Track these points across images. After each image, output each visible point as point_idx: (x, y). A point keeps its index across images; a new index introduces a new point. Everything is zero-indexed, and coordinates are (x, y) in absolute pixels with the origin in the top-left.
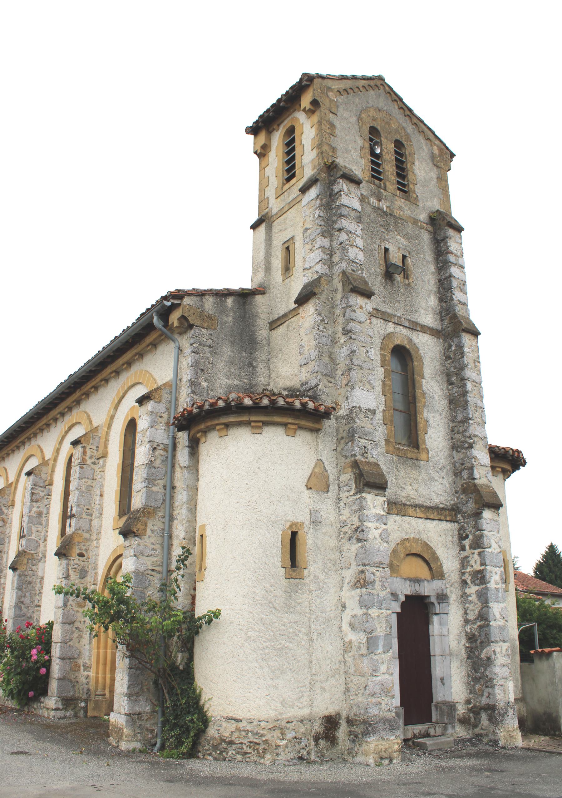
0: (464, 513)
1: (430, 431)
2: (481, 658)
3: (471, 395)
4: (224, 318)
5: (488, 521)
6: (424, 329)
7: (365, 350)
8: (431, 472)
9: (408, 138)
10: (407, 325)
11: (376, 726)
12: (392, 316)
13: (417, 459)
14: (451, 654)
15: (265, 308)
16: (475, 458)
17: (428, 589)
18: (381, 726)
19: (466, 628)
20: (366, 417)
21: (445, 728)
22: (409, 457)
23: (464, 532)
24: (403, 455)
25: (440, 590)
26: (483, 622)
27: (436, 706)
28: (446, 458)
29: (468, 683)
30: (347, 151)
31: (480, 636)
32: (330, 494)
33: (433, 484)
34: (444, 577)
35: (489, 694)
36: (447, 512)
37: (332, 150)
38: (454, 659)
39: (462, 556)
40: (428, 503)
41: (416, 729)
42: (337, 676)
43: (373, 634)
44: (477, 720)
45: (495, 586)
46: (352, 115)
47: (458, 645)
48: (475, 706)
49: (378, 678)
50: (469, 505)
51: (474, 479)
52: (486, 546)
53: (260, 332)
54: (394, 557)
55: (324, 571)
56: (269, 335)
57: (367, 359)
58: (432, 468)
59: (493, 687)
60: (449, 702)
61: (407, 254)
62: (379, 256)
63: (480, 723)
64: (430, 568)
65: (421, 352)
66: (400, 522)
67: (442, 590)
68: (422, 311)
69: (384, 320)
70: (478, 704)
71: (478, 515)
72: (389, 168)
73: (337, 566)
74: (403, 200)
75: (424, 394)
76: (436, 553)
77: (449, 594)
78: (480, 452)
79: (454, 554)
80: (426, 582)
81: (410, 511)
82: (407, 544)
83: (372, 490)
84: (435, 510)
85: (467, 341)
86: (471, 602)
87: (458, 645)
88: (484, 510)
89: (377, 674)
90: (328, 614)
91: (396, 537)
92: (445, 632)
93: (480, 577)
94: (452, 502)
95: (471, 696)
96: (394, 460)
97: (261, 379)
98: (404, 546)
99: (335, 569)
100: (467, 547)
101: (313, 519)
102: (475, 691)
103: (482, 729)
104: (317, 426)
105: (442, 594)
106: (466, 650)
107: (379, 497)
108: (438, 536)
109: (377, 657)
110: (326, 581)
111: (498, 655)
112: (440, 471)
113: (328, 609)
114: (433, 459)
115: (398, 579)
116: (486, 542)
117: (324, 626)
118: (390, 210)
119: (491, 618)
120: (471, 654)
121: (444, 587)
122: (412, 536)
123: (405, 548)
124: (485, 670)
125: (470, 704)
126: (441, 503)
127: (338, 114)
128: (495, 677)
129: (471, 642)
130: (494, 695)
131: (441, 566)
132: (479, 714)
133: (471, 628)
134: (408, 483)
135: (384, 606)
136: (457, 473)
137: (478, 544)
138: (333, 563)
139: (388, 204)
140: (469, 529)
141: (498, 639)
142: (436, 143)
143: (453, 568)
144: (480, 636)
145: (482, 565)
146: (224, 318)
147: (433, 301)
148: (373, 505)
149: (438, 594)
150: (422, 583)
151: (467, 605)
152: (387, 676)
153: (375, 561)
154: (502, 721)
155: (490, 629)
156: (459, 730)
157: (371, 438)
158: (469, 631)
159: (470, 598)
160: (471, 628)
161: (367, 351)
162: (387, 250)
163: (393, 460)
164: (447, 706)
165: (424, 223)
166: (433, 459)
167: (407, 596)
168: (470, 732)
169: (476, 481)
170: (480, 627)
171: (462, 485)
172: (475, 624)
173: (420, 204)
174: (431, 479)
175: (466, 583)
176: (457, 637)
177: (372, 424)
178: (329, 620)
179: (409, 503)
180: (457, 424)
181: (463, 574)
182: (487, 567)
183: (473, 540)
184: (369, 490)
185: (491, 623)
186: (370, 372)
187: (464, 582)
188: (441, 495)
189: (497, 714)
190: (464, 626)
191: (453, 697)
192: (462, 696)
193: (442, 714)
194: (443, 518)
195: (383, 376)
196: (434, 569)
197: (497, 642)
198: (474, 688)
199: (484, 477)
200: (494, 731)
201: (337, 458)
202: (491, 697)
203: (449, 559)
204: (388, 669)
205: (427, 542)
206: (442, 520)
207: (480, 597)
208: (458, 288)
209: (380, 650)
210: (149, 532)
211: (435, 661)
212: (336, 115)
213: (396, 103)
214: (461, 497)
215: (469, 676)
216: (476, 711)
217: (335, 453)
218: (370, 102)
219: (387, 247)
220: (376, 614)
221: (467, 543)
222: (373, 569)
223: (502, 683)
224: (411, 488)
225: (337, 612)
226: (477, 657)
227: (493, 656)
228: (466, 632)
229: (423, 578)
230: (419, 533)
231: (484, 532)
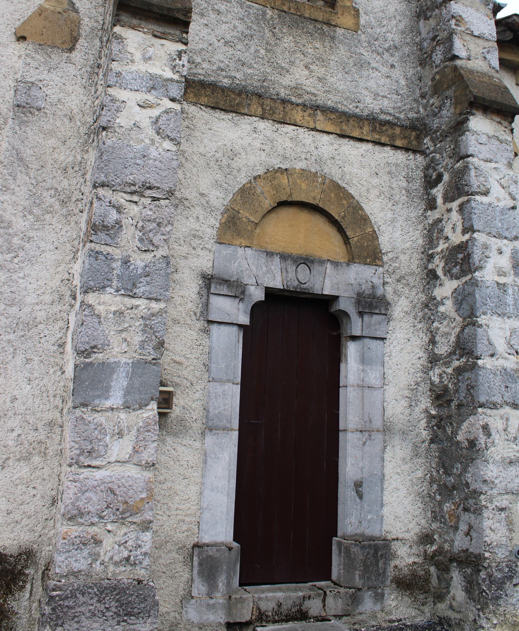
0: (436, 132)
2: (458, 443)
5: (484, 139)
8: (362, 51)
11: (70, 603)
13: (328, 24)
14: (387, 429)
16: (459, 20)
18: (87, 604)
19: (431, 373)
21: (355, 600)
22: (307, 15)
23: (435, 170)
24: (292, 11)
25: (366, 288)
26: (464, 360)
27: (339, 544)
28: (403, 32)
29: (430, 496)
31: (457, 391)
32: (77, 55)
33: (365, 73)
34: (381, 259)
35: (470, 527)
36: (398, 131)
38: (397, 441)
39: (431, 222)
40: (350, 108)
41: (267, 599)
42: (36, 459)
43: (94, 356)
44: (443, 585)
45: (497, 278)
47: (408, 411)
48: (440, 551)
49: (99, 474)
50: (444, 112)
51: (456, 57)
52: (475, 189)
54: (244, 203)
55: (30, 213)
58: (365, 44)
59: (478, 511)
60: (372, 539)
63: (449, 592)
64: (346, 240)
66: (268, 133)
67: (373, 287)
70: (446, 546)
71: (459, 127)
73: (72, 206)
76: (361, 208)
77: (390, 296)
79: (412, 215)
80: (329, 265)
81: (298, 115)
82: (284, 180)
83: (143, 24)
84: (366, 123)
86: (444, 317)
87: (408, 411)
88: (473, 114)
89: (94, 463)
90: (27, 310)
92: (373, 377)
93: (462, 261)
94: (411, 115)
95: (434, 526)
96: (268, 16)
98: (276, 182)
99: (64, 211)
100: (440, 201)
101: (22, 99)
102: (443, 517)
103: (451, 607)
105: (373, 296)
106: (428, 422)
107: (163, 42)
108: (374, 178)
109: (100, 418)
110: (31, 234)
111: (495, 436)
113: (31, 299)
115: (249, 251)
116: (474, 180)
117: (12, 337)
119: (481, 348)
120: (439, 432)
121: (376, 281)
122: (300, 165)
123: (277, 188)
124: (465, 470)
125: (432, 543)
126: (382, 112)
128: (485, 488)
129: (440, 406)
130: (481, 532)
131: (374, 236)
132: (447, 570)
133: (440, 375)
135: (140, 290)
136: (424, 60)
137: (459, 189)
138: (62, 198)
140: (444, 162)
141: (497, 399)
143: (408, 245)
144: (457, 391)
145: (465, 231)
148: (143, 55)
149: (359, 294)
150: (316, 268)
151: (436, 324)
152: (132, 471)
153: (130, 179)
154: (498, 598)
155: (477, 375)
156: (394, 604)
158: (436, 379)
159: (442, 309)
160: (440, 375)
163: (264, 14)
164: (363, 547)
167: (269, 292)
168: (426, 609)
169: (458, 63)
170: (459, 371)
172: (447, 364)
174: (361, 64)
175: (436, 277)
176: (406, 393)
178: (30, 325)
179: (300, 101)
181: (431, 257)
182: (475, 235)
183: (451, 181)
184: (135, 22)
185: (480, 362)
187: (432, 276)
188: (384, 97)
189: (484, 580)
190: (426, 371)
191: (385, 528)
192: (411, 526)
193: (349, 565)
194: (383, 140)
196: (353, 241)
197: (494, 406)
198: (442, 510)
200: (475, 620)
202: (474, 534)
203: (398, 225)
204: (136, 451)
205: (340, 182)
206: (384, 145)
207: (461, 304)
209: (116, 399)
211: (346, 441)
215: (432, 481)
216: (443, 561)
220: (113, 308)
221: (438, 192)
222: (121, 198)
223: (504, 503)
224: (306, 72)
225: (56, 308)
226: (451, 439)
227: (482, 439)
228: (432, 383)
229: (325, 257)
230: (319, 161)
231: (470, 159)
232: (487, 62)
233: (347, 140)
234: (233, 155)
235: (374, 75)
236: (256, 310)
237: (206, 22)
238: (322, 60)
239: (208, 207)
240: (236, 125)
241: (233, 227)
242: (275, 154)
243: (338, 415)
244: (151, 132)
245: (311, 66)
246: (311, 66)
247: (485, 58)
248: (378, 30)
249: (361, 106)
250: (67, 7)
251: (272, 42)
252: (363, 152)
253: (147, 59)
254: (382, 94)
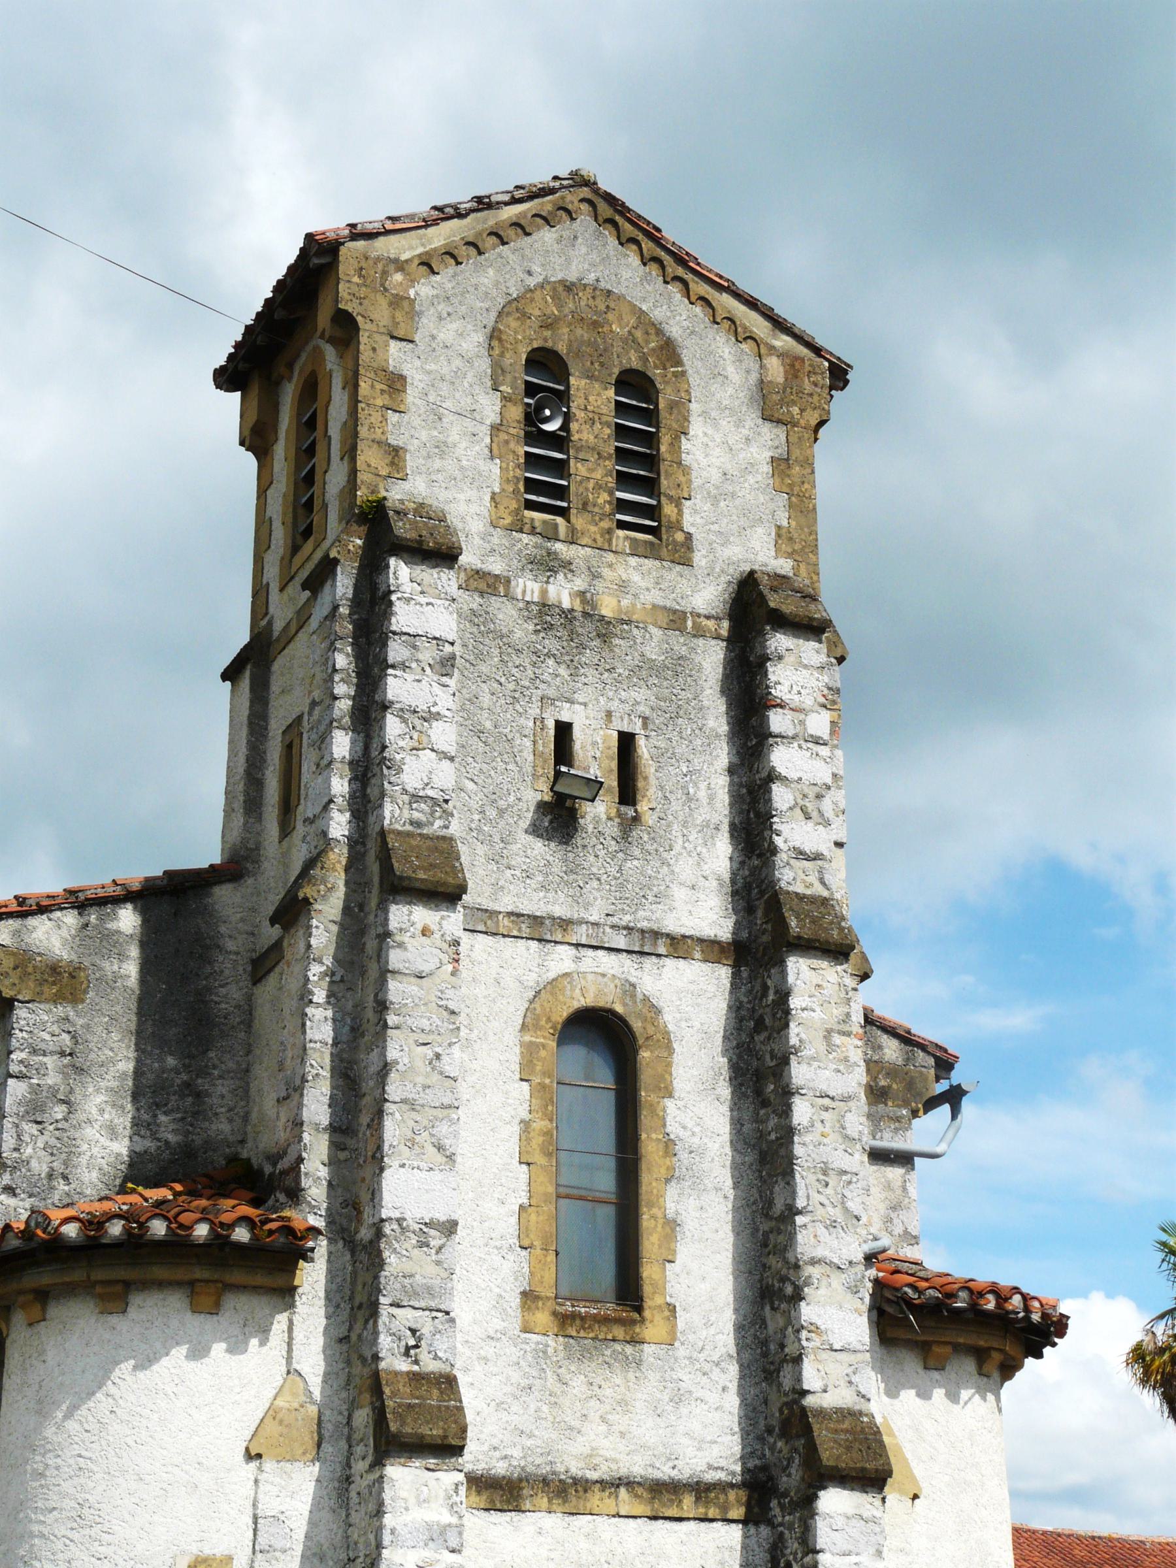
1: (685, 1252)
3: (808, 1138)
4: (110, 967)
6: (679, 946)
7: (430, 1054)
9: (669, 352)
10: (621, 942)
15: (242, 920)
20: (423, 1244)
30: (442, 448)
37: (388, 459)
40: (664, 1472)
46: (470, 327)
53: (223, 991)
56: (249, 998)
57: (435, 1077)
61: (636, 727)
62: (532, 748)
69: (540, 940)
74: (633, 561)
75: (669, 1146)
78: (832, 1310)
85: (806, 973)
96: (550, 1351)
97: (222, 1126)
104: (279, 1281)
112: (716, 1370)
114: (691, 1337)
118: (584, 601)
127: (417, 339)
134: (594, 1416)
139: (580, 584)
142: (777, 343)
146: (110, 967)
147: (720, 855)
157: (433, 1304)
161: (438, 1056)
165: (708, 617)
166: (691, 1337)
171: (781, 1411)
177: (438, 1263)
180: (773, 1223)
186: (439, 1113)
195: (526, 1106)
199: (843, 1383)
201: (348, 1362)
206: (712, 1520)
208: (798, 811)
212: (412, 342)
213: (634, 247)
214: (780, 1444)
217: (345, 1347)
218: (536, 268)
219: (565, 717)
232: (853, 1388)
233: (661, 1522)
235: (698, 1411)
237: (470, 1380)
238: (623, 1404)
240: (516, 1529)
242: (567, 1562)
243: (1094, 1542)
245: (609, 1416)
246: (609, 1416)
247: (850, 1382)
248: (704, 1333)
249: (680, 1464)
250: (304, 1399)
251: (558, 1388)
252: (684, 1537)
253: (422, 1502)
254: (709, 1438)
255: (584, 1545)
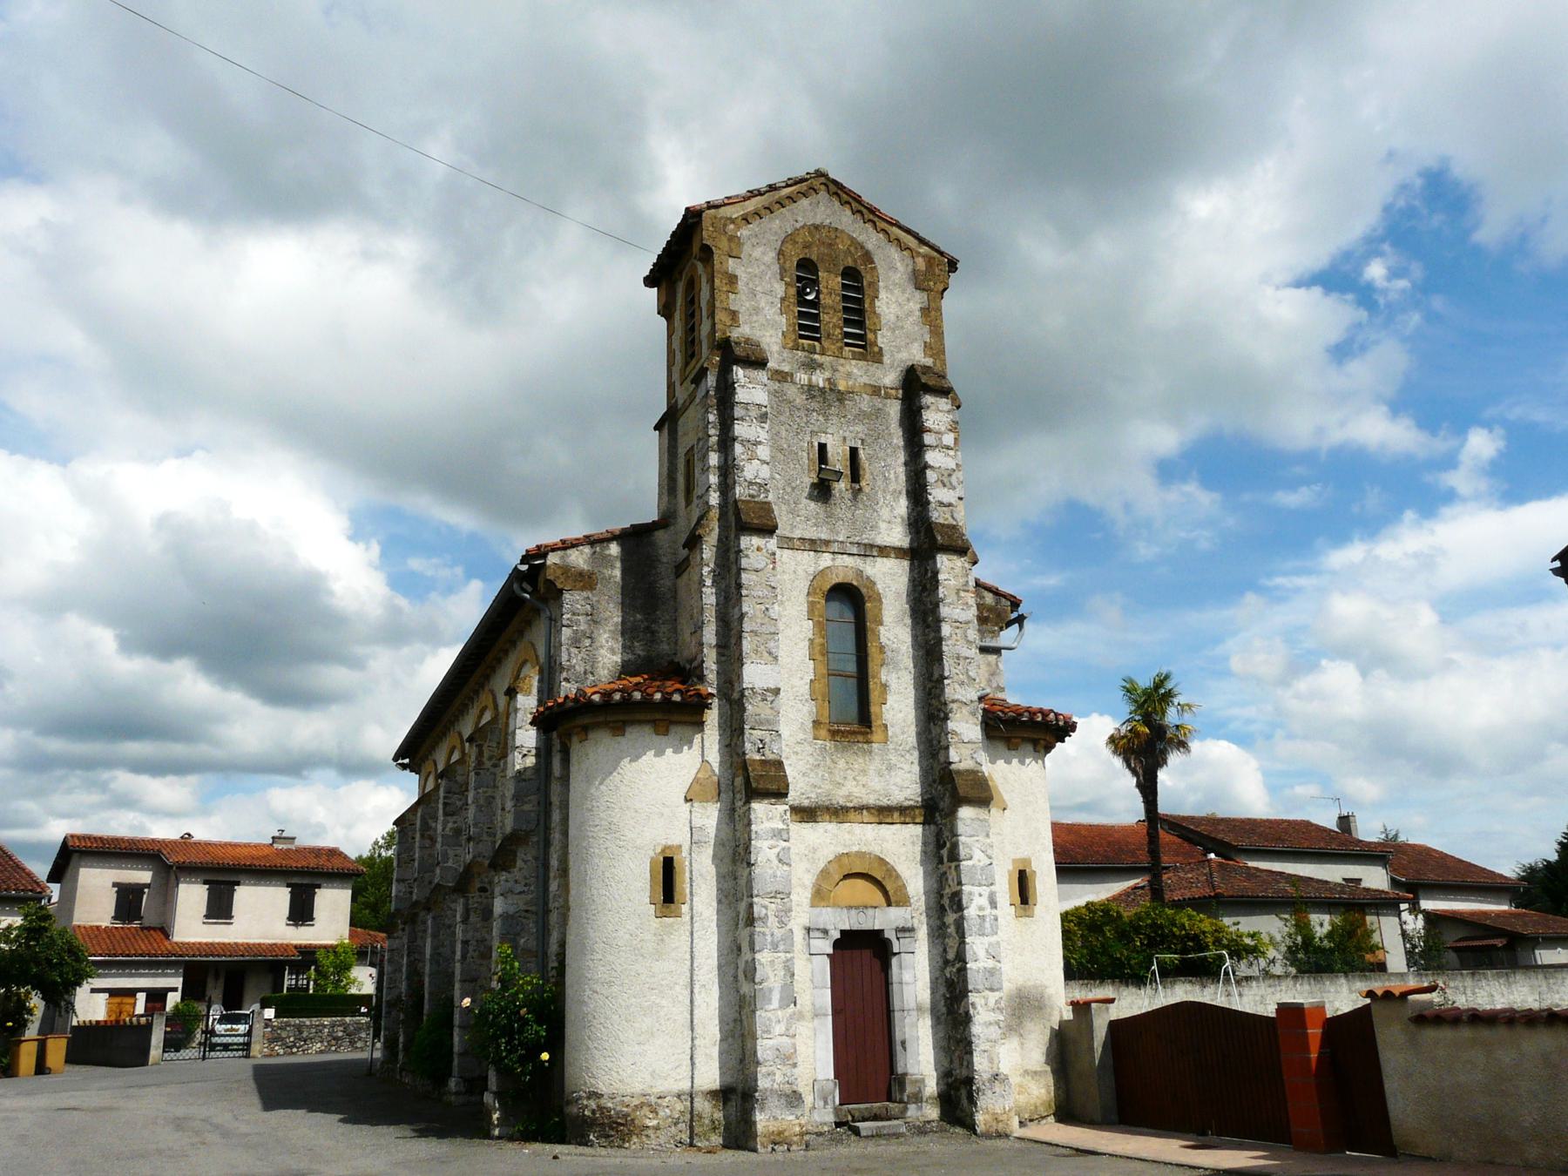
1: (891, 699)
4: (607, 572)
6: (884, 551)
12: (827, 543)
17: (884, 919)
40: (885, 802)
56: (675, 585)
62: (807, 458)
65: (880, 587)
68: (883, 526)
72: (832, 320)
75: (882, 649)
85: (946, 562)
91: (828, 853)
104: (694, 719)
116: (963, 852)
122: (855, 849)
135: (781, 948)
139: (827, 374)
146: (607, 572)
147: (902, 506)
162: (822, 448)
167: (842, 932)
173: (886, 359)
174: (890, 768)
190: (942, 970)
210: (519, 863)
222: (766, 902)
234: (815, 850)
236: (837, 944)
239: (804, 887)
241: (820, 896)
244: (776, 862)
253: (769, 819)
255: (847, 836)
